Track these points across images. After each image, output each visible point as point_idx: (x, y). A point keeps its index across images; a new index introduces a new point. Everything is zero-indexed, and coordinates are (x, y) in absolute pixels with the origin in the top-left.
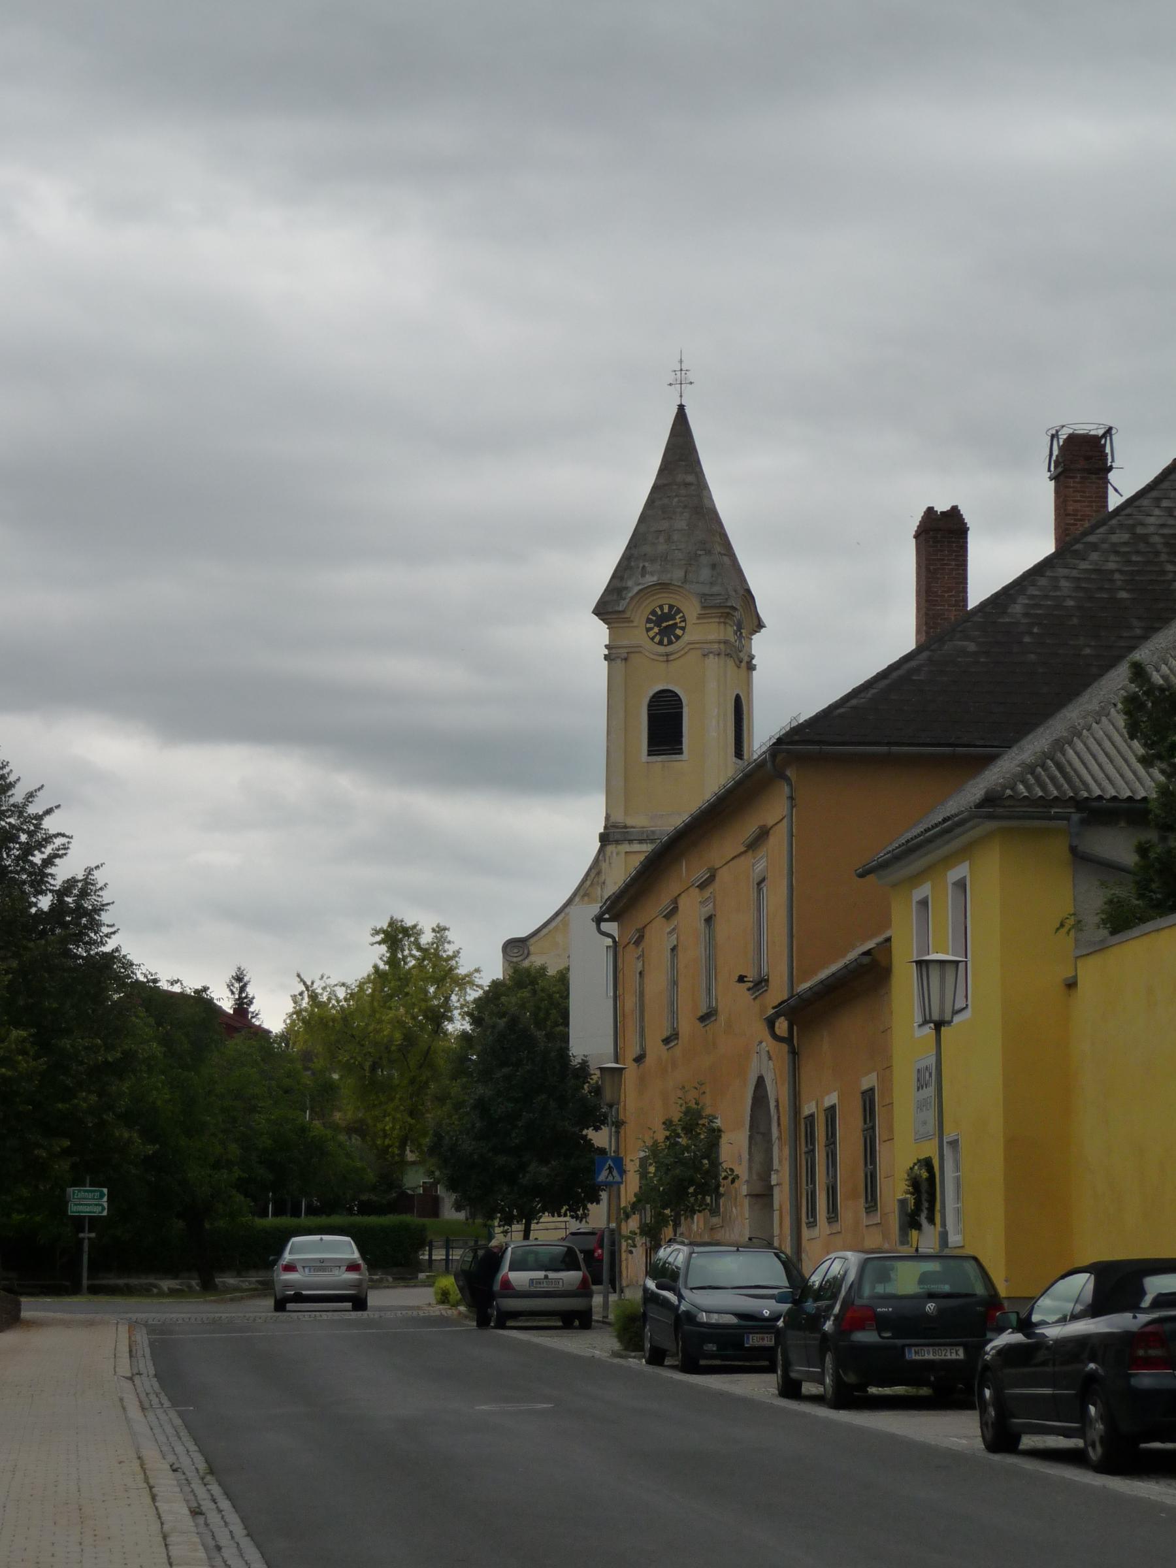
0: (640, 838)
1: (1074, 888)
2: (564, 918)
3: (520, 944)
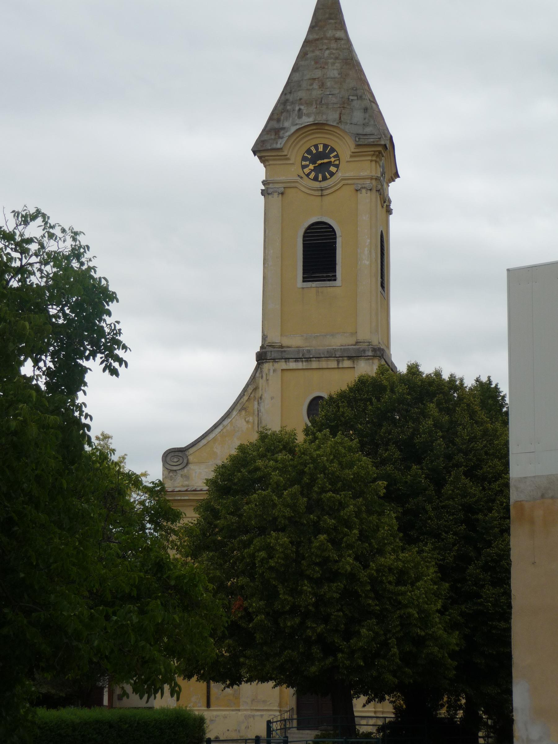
3: (180, 454)
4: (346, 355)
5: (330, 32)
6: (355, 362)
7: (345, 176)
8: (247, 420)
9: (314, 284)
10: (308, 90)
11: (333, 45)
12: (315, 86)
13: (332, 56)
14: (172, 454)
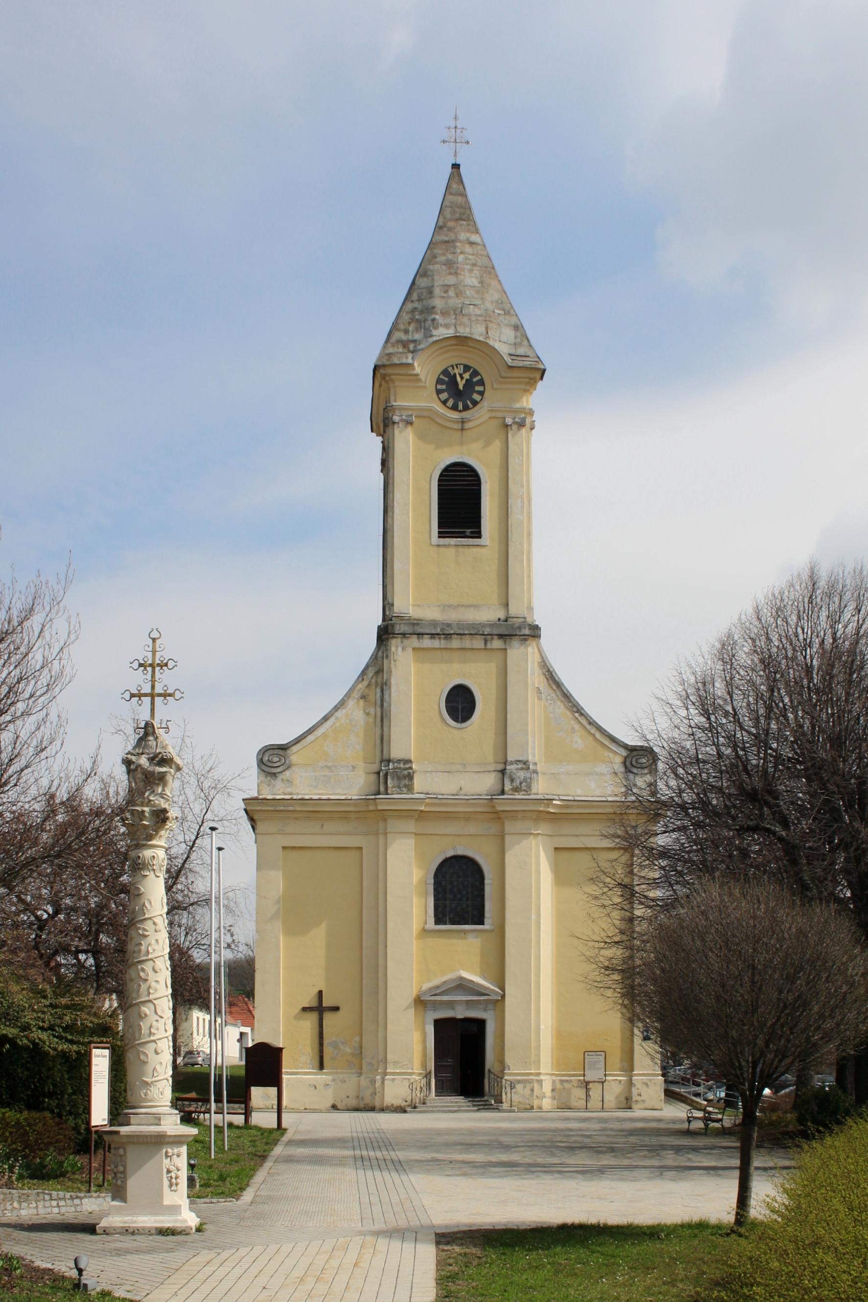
0: (433, 632)
1: (253, 828)
2: (334, 723)
3: (281, 752)
4: (495, 632)
5: (463, 234)
6: (507, 642)
7: (494, 406)
8: (367, 711)
9: (453, 541)
10: (443, 297)
11: (468, 249)
12: (451, 293)
13: (468, 261)
14: (271, 752)
